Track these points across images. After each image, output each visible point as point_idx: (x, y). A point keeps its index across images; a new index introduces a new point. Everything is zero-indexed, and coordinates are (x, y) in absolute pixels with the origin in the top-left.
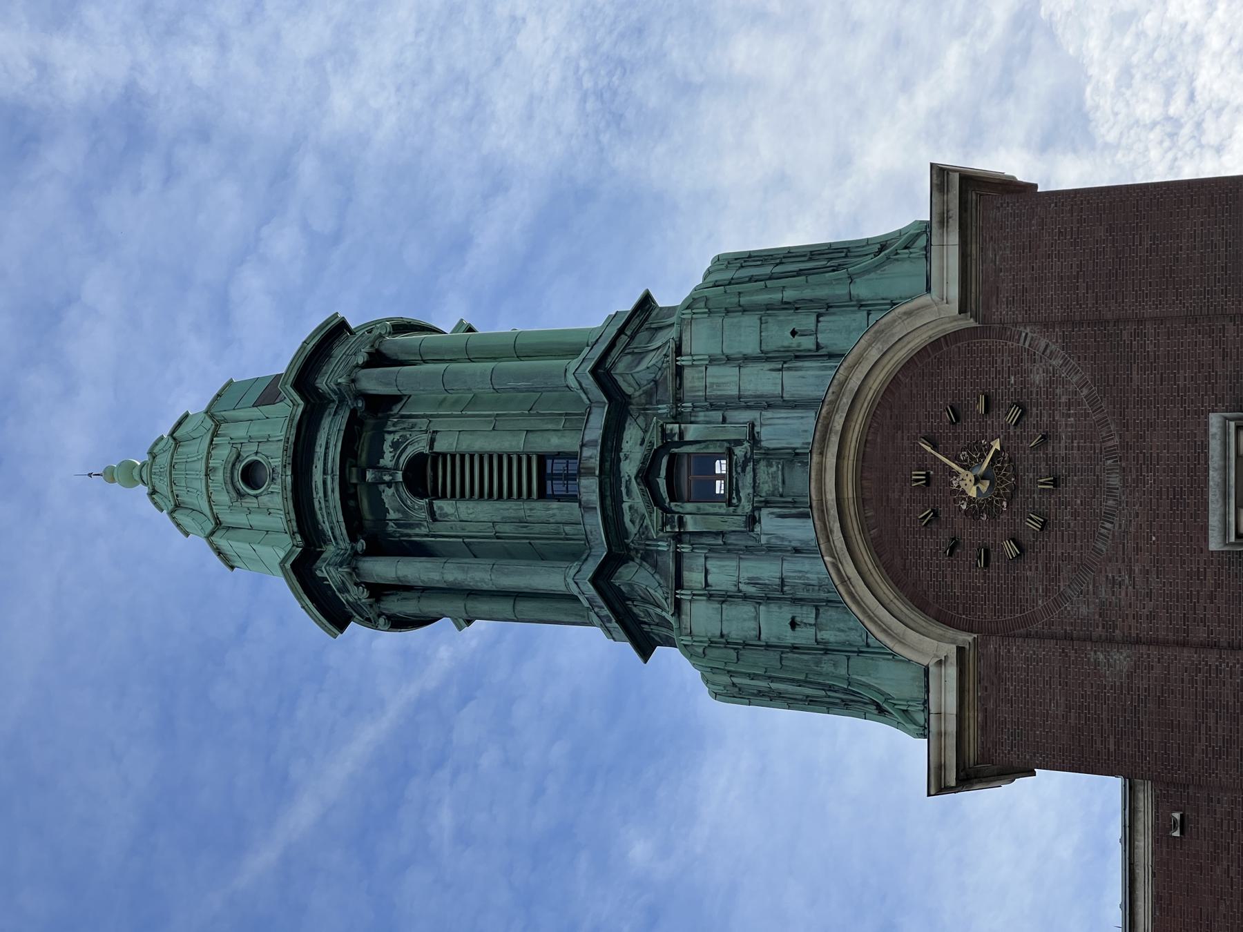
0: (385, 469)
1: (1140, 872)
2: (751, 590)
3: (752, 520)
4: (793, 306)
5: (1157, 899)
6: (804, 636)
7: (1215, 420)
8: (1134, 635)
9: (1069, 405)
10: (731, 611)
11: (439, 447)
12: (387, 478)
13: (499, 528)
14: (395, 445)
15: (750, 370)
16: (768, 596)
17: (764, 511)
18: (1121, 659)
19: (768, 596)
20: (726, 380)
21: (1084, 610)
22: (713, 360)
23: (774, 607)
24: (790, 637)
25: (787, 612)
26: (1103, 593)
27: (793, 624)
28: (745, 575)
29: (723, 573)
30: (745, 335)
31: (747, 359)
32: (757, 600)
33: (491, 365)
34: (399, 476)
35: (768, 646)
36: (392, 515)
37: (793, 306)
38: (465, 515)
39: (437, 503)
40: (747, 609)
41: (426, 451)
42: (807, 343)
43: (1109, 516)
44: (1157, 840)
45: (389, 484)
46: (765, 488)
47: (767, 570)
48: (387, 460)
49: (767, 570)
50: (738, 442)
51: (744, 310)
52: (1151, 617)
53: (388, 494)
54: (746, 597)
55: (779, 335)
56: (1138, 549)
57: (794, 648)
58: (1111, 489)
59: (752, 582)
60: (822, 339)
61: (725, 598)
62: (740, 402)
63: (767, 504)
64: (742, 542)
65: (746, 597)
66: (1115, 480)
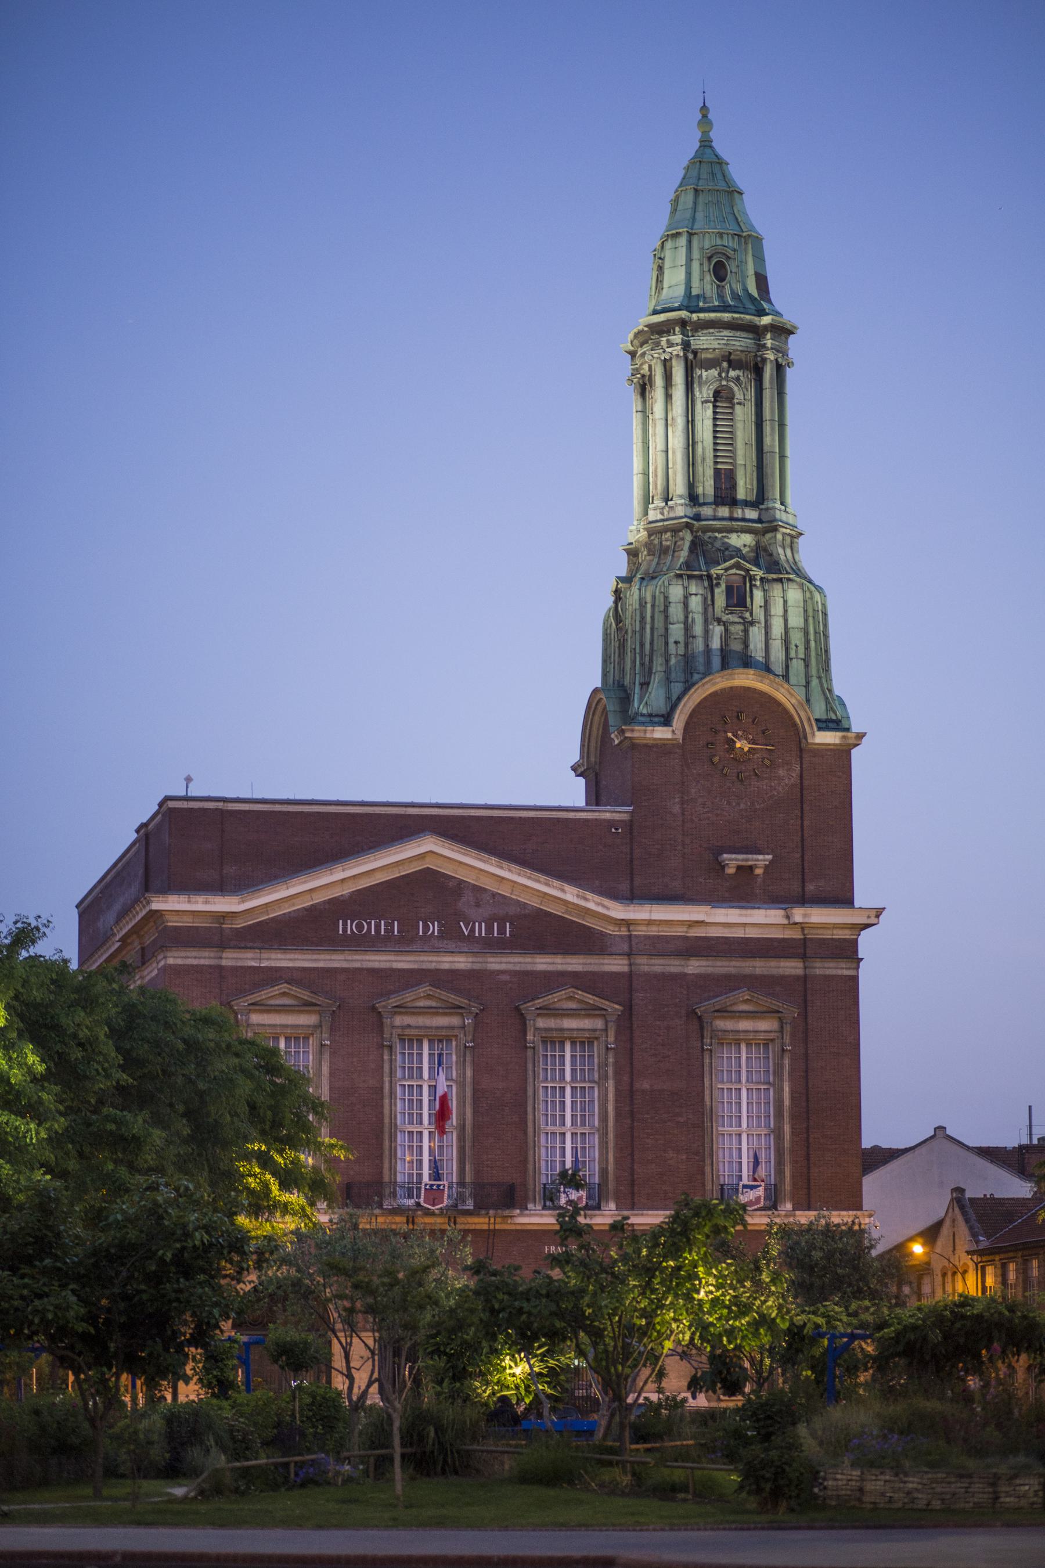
0: (728, 372)
1: (597, 814)
2: (690, 620)
3: (719, 621)
4: (807, 648)
5: (587, 820)
6: (672, 647)
7: (770, 857)
8: (743, 1199)
9: (771, 786)
10: (680, 607)
11: (737, 407)
12: (723, 375)
13: (700, 444)
14: (738, 378)
15: (781, 620)
16: (688, 628)
17: (723, 628)
18: (677, 809)
19: (688, 628)
20: (777, 609)
21: (693, 791)
22: (785, 602)
23: (682, 632)
24: (671, 640)
25: (681, 639)
26: (700, 800)
27: (676, 643)
28: (696, 616)
29: (695, 603)
30: (796, 620)
31: (786, 621)
32: (686, 622)
33: (777, 450)
34: (724, 383)
35: (667, 629)
36: (705, 374)
37: (807, 648)
38: (705, 416)
39: (711, 405)
40: (681, 617)
41: (736, 401)
42: (793, 654)
43: (729, 803)
44: (609, 821)
45: (720, 374)
46: (732, 628)
47: (698, 629)
48: (733, 374)
49: (698, 629)
50: (751, 614)
51: (806, 621)
52: (692, 820)
53: (714, 372)
54: (686, 617)
55: (796, 638)
56: (717, 815)
57: (667, 643)
58: (739, 804)
59: (693, 620)
60: (794, 661)
61: (686, 605)
62: (767, 615)
63: (726, 630)
64: (710, 615)
65: (686, 617)
66: (742, 806)
